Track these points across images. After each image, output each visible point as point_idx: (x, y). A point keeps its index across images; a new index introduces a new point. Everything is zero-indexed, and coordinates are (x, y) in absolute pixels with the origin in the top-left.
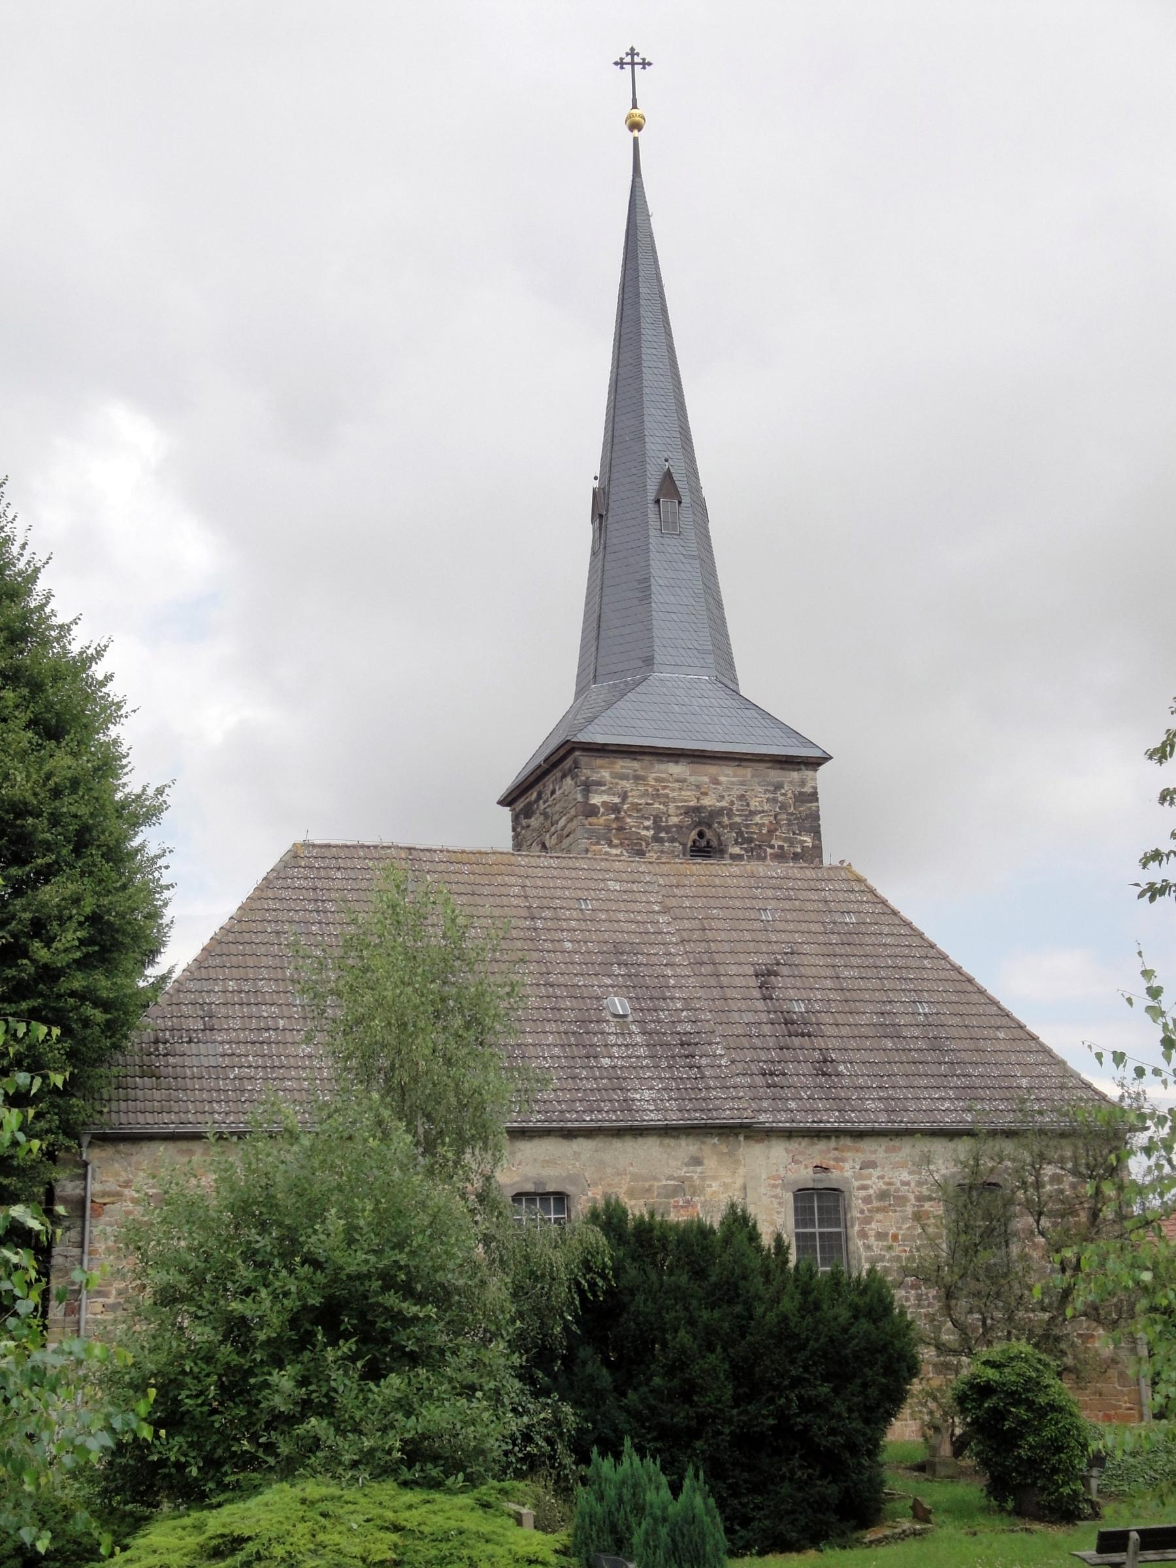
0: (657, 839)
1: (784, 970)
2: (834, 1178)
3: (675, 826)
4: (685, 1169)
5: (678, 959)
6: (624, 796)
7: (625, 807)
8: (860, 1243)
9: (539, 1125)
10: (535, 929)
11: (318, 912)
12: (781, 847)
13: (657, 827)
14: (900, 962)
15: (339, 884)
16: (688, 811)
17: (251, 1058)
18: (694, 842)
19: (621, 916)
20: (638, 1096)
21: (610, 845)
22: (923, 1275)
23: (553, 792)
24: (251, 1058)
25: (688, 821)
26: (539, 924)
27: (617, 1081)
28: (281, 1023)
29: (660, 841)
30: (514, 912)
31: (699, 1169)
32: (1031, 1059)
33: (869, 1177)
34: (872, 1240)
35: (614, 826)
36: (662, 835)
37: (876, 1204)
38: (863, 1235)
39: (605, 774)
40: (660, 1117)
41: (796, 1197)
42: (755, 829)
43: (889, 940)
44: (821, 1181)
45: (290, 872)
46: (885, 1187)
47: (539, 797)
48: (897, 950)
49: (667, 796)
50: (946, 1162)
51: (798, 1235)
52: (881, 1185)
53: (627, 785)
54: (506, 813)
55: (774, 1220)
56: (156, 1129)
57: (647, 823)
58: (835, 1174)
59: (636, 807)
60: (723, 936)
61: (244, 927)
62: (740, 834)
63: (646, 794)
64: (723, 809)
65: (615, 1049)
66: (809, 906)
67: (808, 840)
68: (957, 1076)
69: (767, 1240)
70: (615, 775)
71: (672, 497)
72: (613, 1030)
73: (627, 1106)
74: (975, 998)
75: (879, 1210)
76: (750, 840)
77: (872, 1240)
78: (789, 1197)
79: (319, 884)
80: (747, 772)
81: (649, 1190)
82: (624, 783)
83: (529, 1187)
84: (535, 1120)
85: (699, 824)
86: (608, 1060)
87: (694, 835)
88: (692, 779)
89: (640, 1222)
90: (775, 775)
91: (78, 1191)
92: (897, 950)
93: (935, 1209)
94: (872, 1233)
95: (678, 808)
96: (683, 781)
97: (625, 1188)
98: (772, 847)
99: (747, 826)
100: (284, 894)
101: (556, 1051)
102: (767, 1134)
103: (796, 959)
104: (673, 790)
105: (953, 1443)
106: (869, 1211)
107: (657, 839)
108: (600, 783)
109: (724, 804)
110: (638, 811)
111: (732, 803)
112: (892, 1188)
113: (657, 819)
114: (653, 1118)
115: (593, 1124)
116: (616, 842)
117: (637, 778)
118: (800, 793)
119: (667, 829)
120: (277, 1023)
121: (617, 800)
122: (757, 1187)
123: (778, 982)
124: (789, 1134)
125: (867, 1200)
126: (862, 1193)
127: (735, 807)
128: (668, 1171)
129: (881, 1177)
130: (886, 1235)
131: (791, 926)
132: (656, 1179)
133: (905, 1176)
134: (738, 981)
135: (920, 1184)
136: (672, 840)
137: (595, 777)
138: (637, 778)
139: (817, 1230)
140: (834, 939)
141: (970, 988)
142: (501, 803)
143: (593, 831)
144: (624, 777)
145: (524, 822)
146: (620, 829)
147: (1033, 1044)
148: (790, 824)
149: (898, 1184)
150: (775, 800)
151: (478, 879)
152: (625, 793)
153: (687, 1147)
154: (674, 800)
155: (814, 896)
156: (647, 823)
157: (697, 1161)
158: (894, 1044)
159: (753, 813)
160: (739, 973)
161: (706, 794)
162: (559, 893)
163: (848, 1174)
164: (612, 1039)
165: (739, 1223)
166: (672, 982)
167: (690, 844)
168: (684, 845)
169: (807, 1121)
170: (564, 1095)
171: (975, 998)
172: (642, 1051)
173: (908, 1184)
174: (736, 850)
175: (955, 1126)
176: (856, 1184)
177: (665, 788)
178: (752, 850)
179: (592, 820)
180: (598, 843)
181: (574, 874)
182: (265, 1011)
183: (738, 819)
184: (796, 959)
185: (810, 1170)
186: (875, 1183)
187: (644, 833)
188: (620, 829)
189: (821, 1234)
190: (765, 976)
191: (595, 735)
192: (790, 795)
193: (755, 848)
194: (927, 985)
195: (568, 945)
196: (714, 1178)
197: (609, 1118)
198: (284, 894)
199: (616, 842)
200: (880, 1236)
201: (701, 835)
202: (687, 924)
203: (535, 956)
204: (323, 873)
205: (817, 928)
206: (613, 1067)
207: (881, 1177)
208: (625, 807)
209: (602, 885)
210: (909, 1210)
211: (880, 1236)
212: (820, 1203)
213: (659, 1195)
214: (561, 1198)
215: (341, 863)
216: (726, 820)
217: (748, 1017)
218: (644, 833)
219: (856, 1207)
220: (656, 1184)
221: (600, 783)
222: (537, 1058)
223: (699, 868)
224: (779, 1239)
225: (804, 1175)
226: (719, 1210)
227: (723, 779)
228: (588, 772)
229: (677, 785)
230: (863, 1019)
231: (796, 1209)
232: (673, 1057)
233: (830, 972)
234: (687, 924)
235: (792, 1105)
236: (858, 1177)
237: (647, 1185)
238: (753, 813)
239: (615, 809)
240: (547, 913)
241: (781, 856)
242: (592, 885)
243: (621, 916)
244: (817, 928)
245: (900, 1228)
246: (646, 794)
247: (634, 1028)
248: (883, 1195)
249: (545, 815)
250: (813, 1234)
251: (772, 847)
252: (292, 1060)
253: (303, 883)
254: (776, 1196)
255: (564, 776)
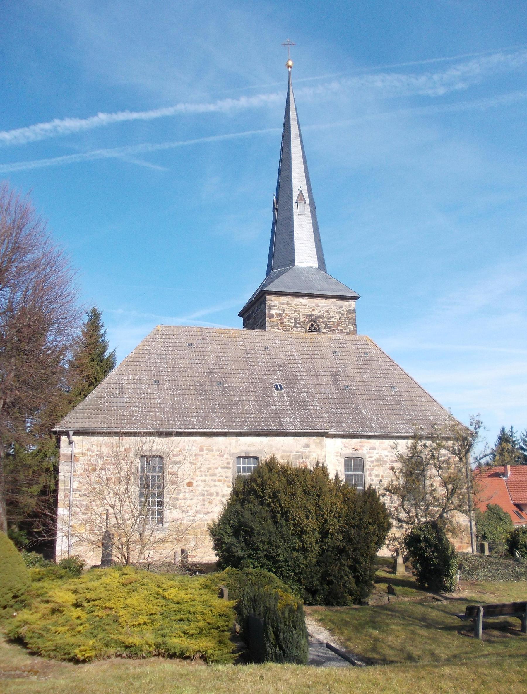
0: (295, 327)
1: (342, 374)
2: (360, 453)
3: (302, 322)
4: (303, 448)
5: (302, 369)
6: (283, 311)
7: (284, 315)
8: (369, 478)
9: (247, 430)
10: (248, 358)
11: (165, 350)
12: (342, 330)
13: (296, 322)
14: (386, 372)
15: (173, 341)
16: (307, 316)
17: (137, 404)
18: (310, 328)
19: (280, 353)
20: (285, 420)
21: (278, 329)
22: (392, 490)
23: (257, 310)
24: (137, 404)
25: (307, 320)
26: (249, 356)
27: (277, 414)
28: (149, 391)
29: (297, 327)
30: (240, 351)
31: (308, 448)
32: (434, 409)
33: (373, 453)
34: (373, 477)
35: (280, 322)
36: (298, 325)
37: (375, 463)
38: (370, 475)
39: (276, 303)
40: (293, 428)
41: (345, 460)
42: (332, 323)
43: (381, 363)
44: (354, 454)
45: (155, 336)
46: (379, 457)
47: (253, 312)
48: (384, 367)
49: (299, 311)
50: (403, 446)
51: (345, 474)
52: (377, 456)
53: (285, 307)
54: (241, 319)
55: (335, 469)
56: (99, 430)
57: (292, 321)
58: (360, 452)
59: (288, 315)
60: (319, 361)
61: (137, 356)
62: (326, 325)
63: (291, 310)
64: (320, 316)
65: (277, 402)
66: (351, 350)
67: (352, 327)
68: (407, 415)
69: (332, 476)
70: (280, 303)
71: (302, 201)
72: (276, 395)
73: (281, 424)
74: (414, 385)
75: (376, 466)
76: (330, 327)
77: (373, 477)
78: (343, 460)
79: (166, 340)
80: (329, 301)
81: (289, 456)
82: (283, 306)
83: (243, 454)
84: (245, 429)
85: (311, 321)
86: (274, 407)
87: (309, 325)
88: (309, 304)
89: (283, 467)
90: (339, 303)
91: (70, 452)
92: (384, 367)
93: (398, 465)
94: (374, 475)
95: (303, 315)
96: (305, 305)
97: (280, 455)
98: (338, 330)
99: (329, 322)
100: (152, 344)
101: (254, 403)
102: (335, 436)
103: (346, 370)
104: (302, 309)
105: (403, 558)
106: (373, 466)
107: (295, 327)
108: (274, 306)
109: (320, 314)
110: (289, 316)
111: (324, 313)
112: (381, 458)
113: (296, 319)
114: (291, 429)
115: (267, 431)
116: (280, 328)
117: (288, 304)
118: (349, 310)
119: (299, 323)
120: (147, 391)
121: (281, 312)
122: (331, 456)
123: (340, 378)
124: (343, 436)
125: (372, 462)
126: (370, 459)
127: (324, 315)
128: (296, 450)
129: (377, 453)
130: (379, 475)
131: (345, 358)
132: (291, 452)
133: (387, 453)
134: (324, 378)
135: (392, 456)
136: (301, 327)
137: (273, 304)
138: (288, 304)
139: (353, 473)
140: (361, 362)
141: (412, 382)
142: (240, 315)
143: (272, 324)
144: (283, 304)
145: (247, 322)
146: (282, 323)
147: (435, 403)
148: (345, 321)
149: (384, 456)
150: (339, 312)
151: (227, 339)
152: (284, 310)
153: (304, 440)
154: (302, 312)
155: (353, 346)
156: (292, 321)
157: (307, 446)
158: (383, 402)
159: (331, 317)
160: (325, 375)
161: (314, 310)
162: (258, 344)
163: (365, 452)
164: (276, 399)
165: (321, 470)
166: (299, 378)
167: (308, 328)
168: (306, 329)
169: (351, 432)
170: (257, 419)
171: (414, 385)
172: (287, 404)
173: (387, 456)
174: (325, 331)
175: (405, 434)
176: (368, 455)
177: (299, 308)
178: (331, 331)
179: (271, 319)
180: (274, 328)
181: (263, 337)
182: (143, 386)
183: (326, 320)
184: (346, 370)
185: (351, 450)
186: (376, 456)
187: (291, 324)
188: (282, 323)
189: (354, 475)
190: (335, 376)
191: (272, 288)
192: (345, 310)
193: (331, 329)
194: (395, 380)
195: (260, 364)
196: (314, 452)
197: (275, 430)
198: (152, 344)
199: (280, 328)
200: (377, 476)
201: (312, 325)
202: (306, 356)
203: (247, 367)
204: (167, 336)
205: (355, 358)
206: (276, 409)
207: (377, 453)
208: (284, 315)
209: (274, 342)
210: (388, 466)
211: (377, 476)
212: (355, 463)
213: (292, 458)
214: (256, 458)
215: (175, 333)
216: (321, 320)
217: (328, 391)
218: (291, 324)
219: (368, 465)
220: (292, 454)
221: (274, 306)
222: (247, 405)
223: (311, 335)
224: (337, 476)
225: (348, 452)
226: (212, 670)
227: (320, 304)
228: (270, 302)
229: (303, 307)
230: (371, 393)
231: (345, 464)
232: (299, 406)
233: (359, 375)
234: (306, 356)
235: (344, 425)
236: (369, 453)
237: (288, 454)
238: (331, 317)
239: (280, 315)
240: (252, 352)
241: (342, 332)
242: (270, 341)
243: (280, 353)
244: (355, 358)
245: (384, 473)
246: (291, 310)
247: (284, 394)
248: (378, 460)
249: (255, 318)
250: (351, 475)
251: (338, 330)
252: (153, 405)
253: (161, 340)
254: (337, 460)
255: (261, 304)
